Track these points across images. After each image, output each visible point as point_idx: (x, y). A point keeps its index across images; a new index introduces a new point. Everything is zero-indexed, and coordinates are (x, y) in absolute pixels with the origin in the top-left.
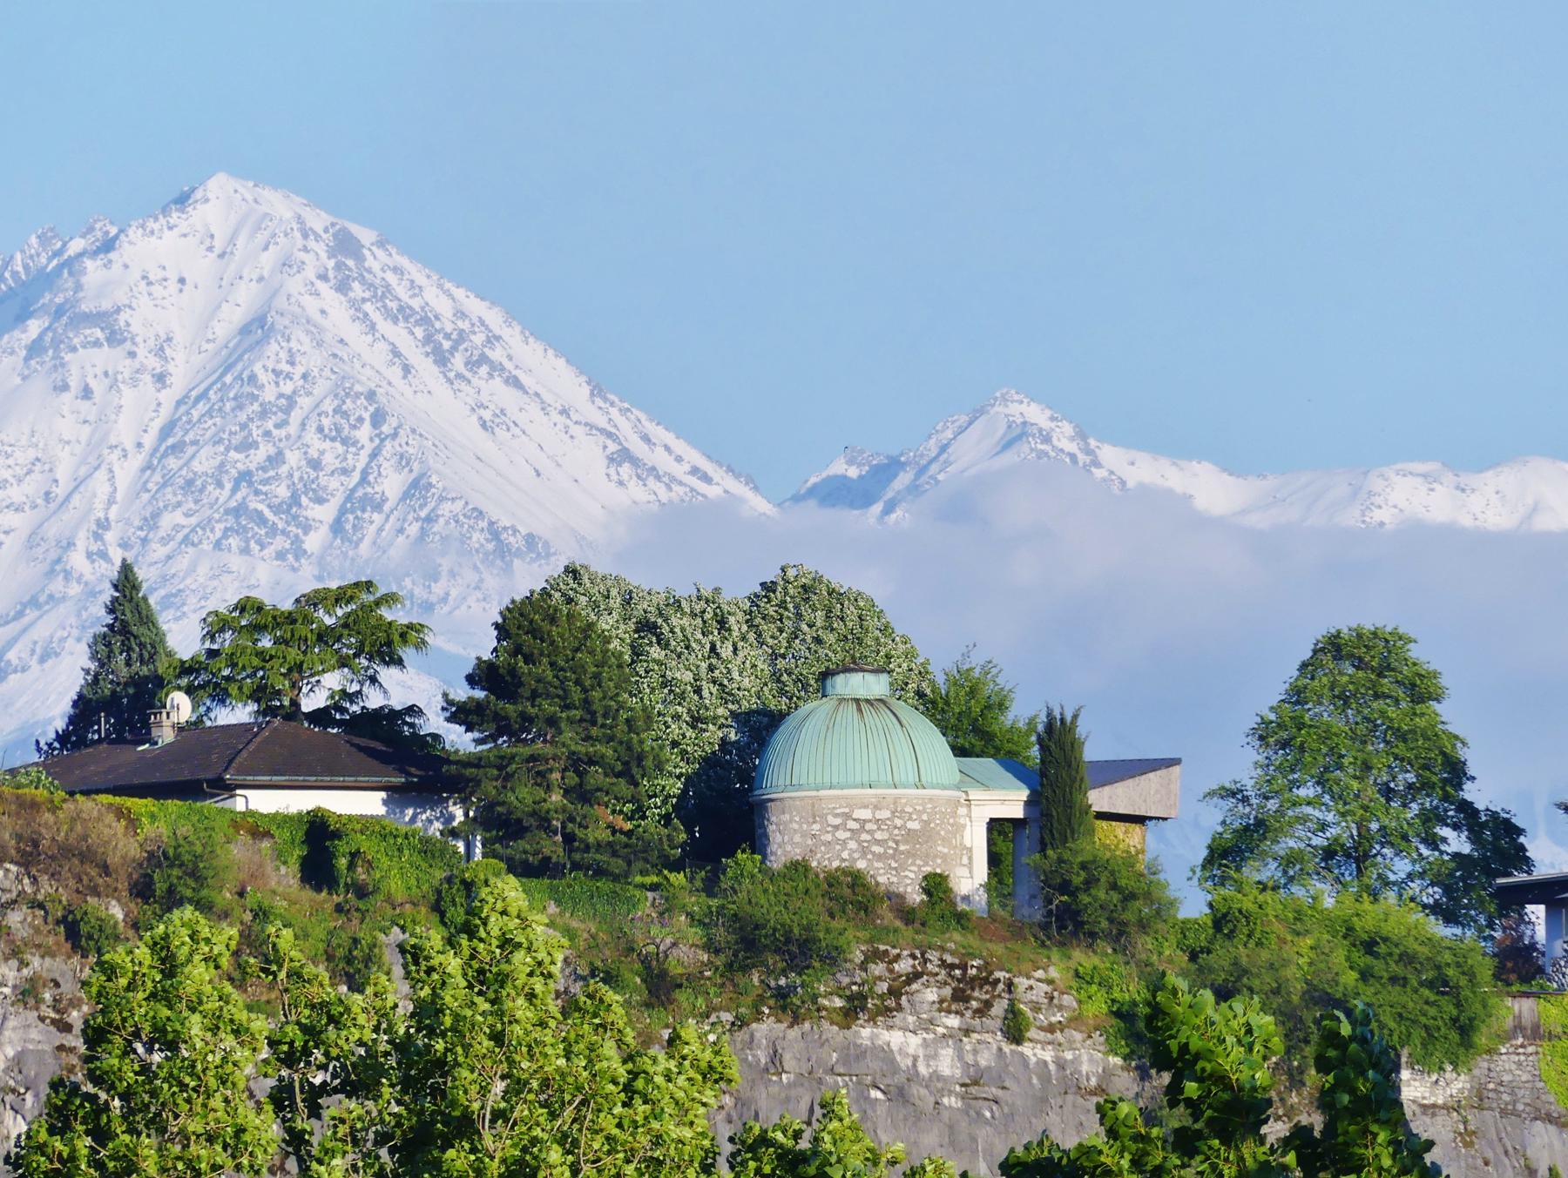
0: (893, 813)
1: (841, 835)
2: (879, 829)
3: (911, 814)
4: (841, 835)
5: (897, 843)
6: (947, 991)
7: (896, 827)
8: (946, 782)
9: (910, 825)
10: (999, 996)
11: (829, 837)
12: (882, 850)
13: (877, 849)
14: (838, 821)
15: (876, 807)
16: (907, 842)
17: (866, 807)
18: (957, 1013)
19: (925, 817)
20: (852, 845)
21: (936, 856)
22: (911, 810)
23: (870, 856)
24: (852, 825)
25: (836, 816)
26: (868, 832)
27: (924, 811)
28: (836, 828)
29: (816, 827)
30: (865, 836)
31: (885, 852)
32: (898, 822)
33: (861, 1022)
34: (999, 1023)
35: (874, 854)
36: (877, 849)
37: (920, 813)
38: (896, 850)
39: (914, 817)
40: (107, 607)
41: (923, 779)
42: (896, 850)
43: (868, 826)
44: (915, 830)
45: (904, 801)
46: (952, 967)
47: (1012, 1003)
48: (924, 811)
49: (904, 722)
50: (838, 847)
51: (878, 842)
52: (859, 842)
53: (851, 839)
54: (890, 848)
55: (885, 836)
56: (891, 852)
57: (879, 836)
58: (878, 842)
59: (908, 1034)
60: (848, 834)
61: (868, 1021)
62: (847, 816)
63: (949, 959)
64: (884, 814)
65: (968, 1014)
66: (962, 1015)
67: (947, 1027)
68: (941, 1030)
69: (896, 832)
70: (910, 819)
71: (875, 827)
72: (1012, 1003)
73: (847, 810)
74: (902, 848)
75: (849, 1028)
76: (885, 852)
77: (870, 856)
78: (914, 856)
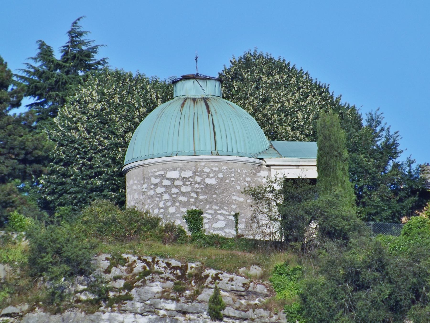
0: (194, 173)
1: (160, 190)
2: (184, 184)
3: (208, 173)
4: (160, 190)
5: (197, 194)
6: (170, 284)
7: (196, 183)
8: (241, 150)
9: (208, 181)
10: (207, 286)
11: (151, 193)
12: (186, 199)
13: (183, 199)
14: (157, 181)
15: (182, 169)
16: (205, 193)
17: (175, 169)
18: (173, 300)
19: (220, 175)
20: (166, 197)
21: (232, 203)
22: (208, 170)
23: (177, 204)
24: (166, 183)
25: (156, 177)
26: (177, 187)
27: (220, 171)
28: (156, 185)
29: (145, 186)
30: (174, 190)
31: (189, 200)
32: (198, 179)
33: (102, 308)
34: (206, 306)
35: (180, 202)
36: (183, 199)
37: (216, 173)
38: (196, 199)
39: (212, 175)
40: (366, 121)
41: (219, 148)
42: (196, 199)
43: (177, 183)
44: (211, 185)
45: (203, 164)
46: (176, 268)
47: (217, 291)
48: (220, 171)
49: (212, 110)
50: (157, 199)
51: (184, 194)
52: (171, 195)
53: (165, 192)
54: (192, 197)
55: (189, 189)
56: (193, 200)
57: (184, 189)
58: (184, 194)
59: (138, 316)
60: (163, 190)
61: (107, 307)
62: (163, 177)
63: (174, 263)
64: (188, 174)
65: (182, 300)
66: (178, 301)
67: (166, 310)
68: (162, 312)
69: (197, 186)
70: (208, 177)
71: (181, 183)
72: (217, 291)
73: (162, 173)
74: (201, 197)
75: (92, 313)
76: (189, 200)
77: (177, 204)
78: (211, 203)
